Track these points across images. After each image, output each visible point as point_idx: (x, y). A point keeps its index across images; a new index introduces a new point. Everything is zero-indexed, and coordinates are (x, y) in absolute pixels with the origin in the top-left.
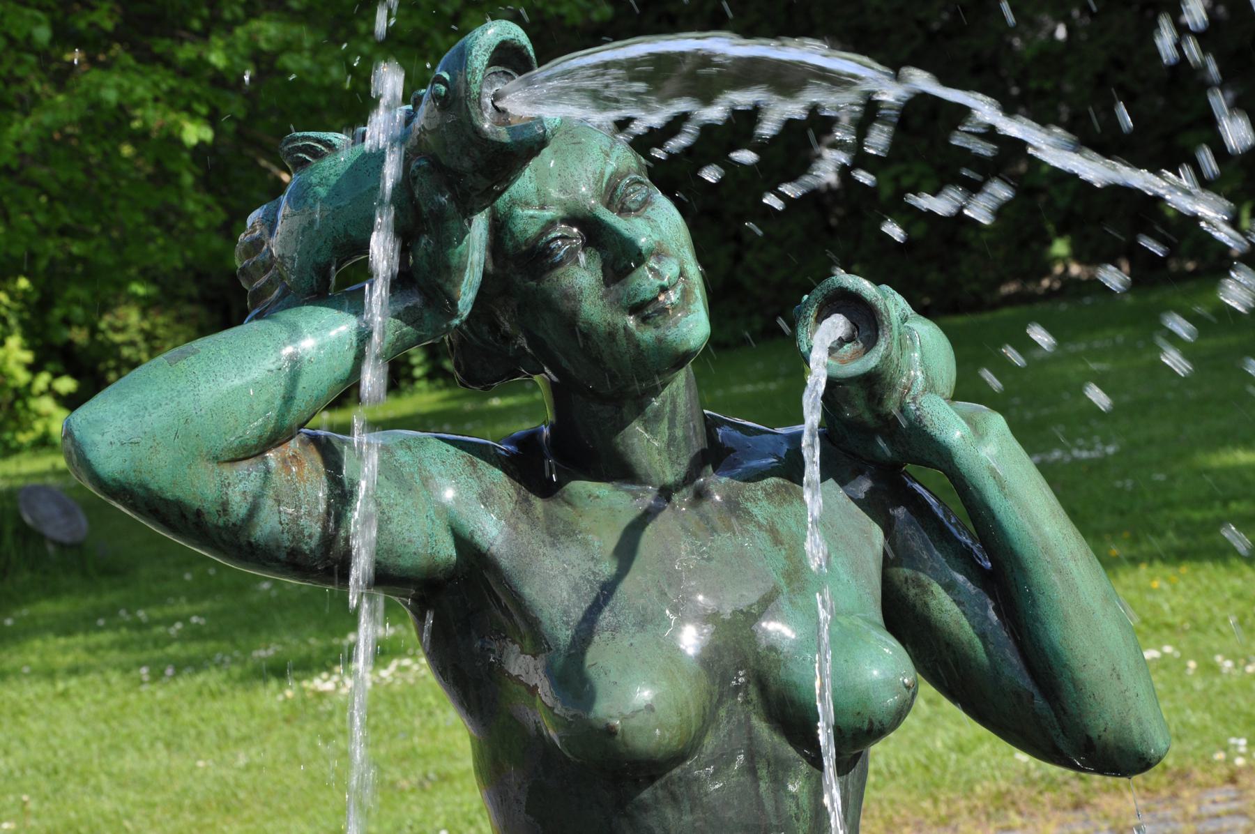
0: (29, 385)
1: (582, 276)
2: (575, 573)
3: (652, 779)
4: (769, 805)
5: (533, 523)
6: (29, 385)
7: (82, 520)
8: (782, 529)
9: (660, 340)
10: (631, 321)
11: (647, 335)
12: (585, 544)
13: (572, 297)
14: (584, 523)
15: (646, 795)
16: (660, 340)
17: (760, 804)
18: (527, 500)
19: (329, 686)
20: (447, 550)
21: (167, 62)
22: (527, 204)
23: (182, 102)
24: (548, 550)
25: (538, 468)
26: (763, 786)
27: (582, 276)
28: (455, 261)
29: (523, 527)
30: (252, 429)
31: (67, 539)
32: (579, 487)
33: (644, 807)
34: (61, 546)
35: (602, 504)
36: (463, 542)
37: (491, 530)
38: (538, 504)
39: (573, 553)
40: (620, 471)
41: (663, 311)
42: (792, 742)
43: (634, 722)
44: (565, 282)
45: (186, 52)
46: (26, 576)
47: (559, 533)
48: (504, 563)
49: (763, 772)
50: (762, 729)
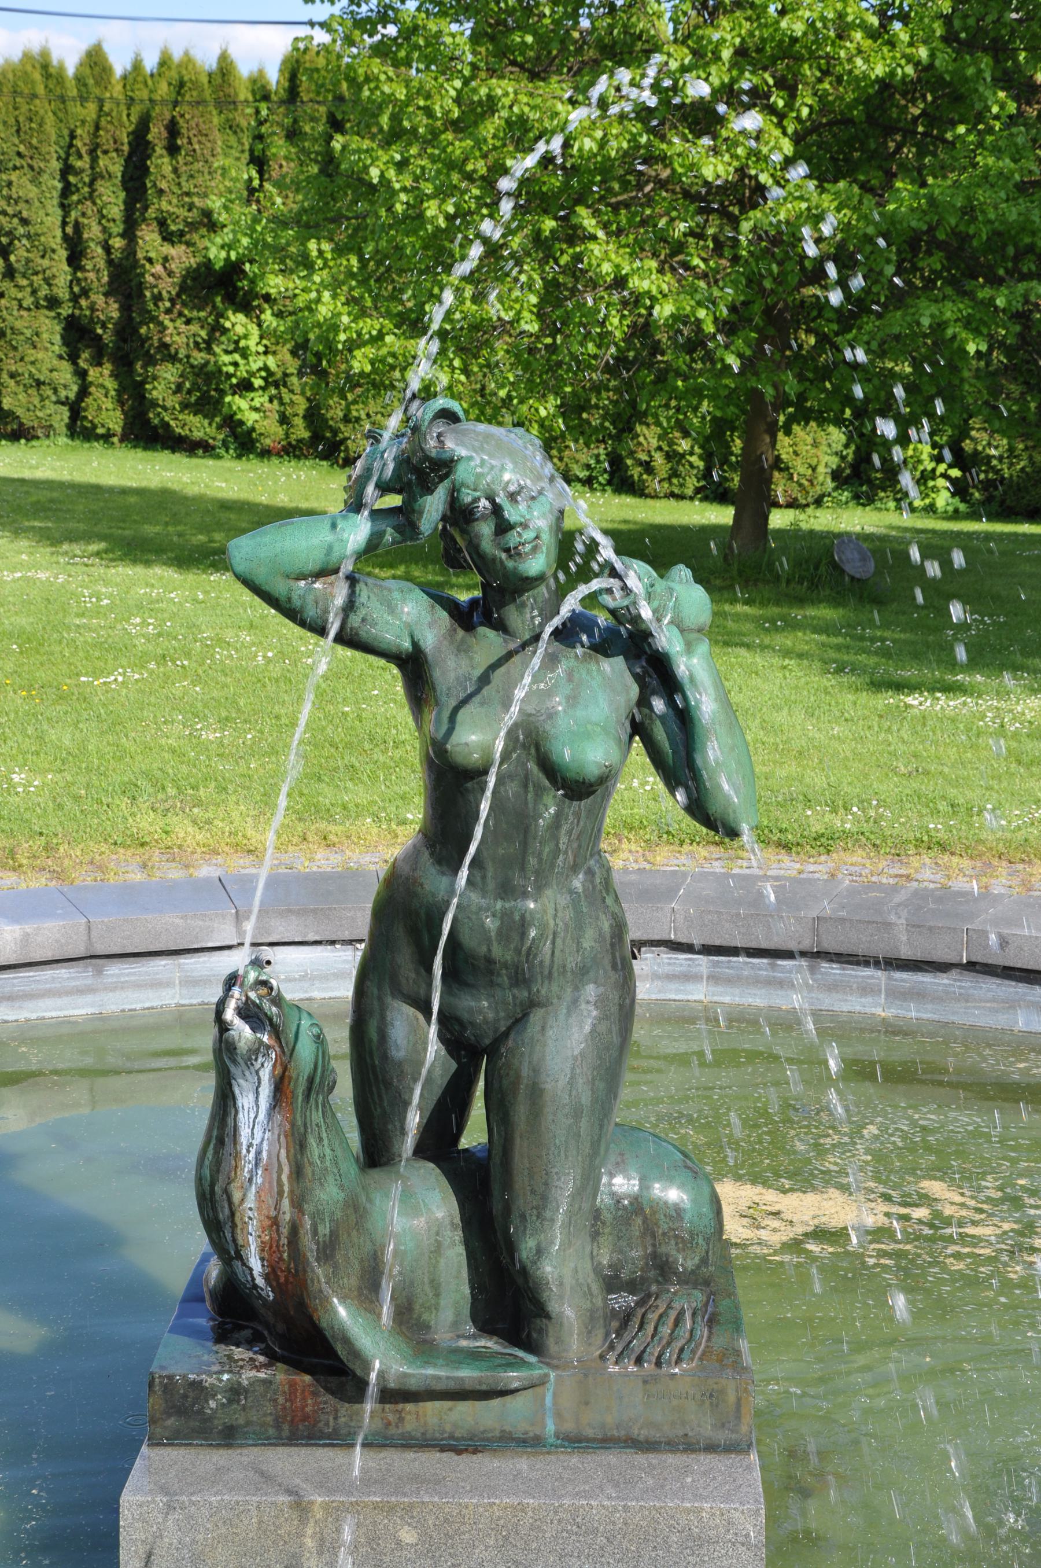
0: (934, 470)
1: (485, 529)
2: (461, 672)
3: (472, 778)
4: (531, 806)
5: (452, 643)
6: (934, 470)
7: (871, 565)
8: (576, 676)
9: (515, 568)
10: (504, 556)
11: (510, 564)
12: (471, 659)
13: (478, 536)
14: (476, 648)
15: (469, 785)
16: (515, 568)
17: (526, 803)
18: (455, 630)
19: (916, 703)
20: (407, 645)
21: (970, 295)
22: (468, 487)
23: (974, 325)
24: (452, 657)
25: (465, 618)
26: (530, 796)
27: (485, 529)
28: (417, 507)
29: (446, 643)
30: (312, 566)
31: (858, 576)
32: (483, 630)
33: (467, 790)
34: (853, 578)
35: (489, 643)
36: (415, 644)
37: (429, 640)
38: (461, 633)
39: (464, 662)
40: (501, 626)
41: (519, 554)
42: (548, 778)
43: (458, 749)
44: (477, 528)
45: (983, 294)
46: (828, 592)
47: (462, 649)
48: (430, 658)
49: (531, 789)
50: (532, 766)
